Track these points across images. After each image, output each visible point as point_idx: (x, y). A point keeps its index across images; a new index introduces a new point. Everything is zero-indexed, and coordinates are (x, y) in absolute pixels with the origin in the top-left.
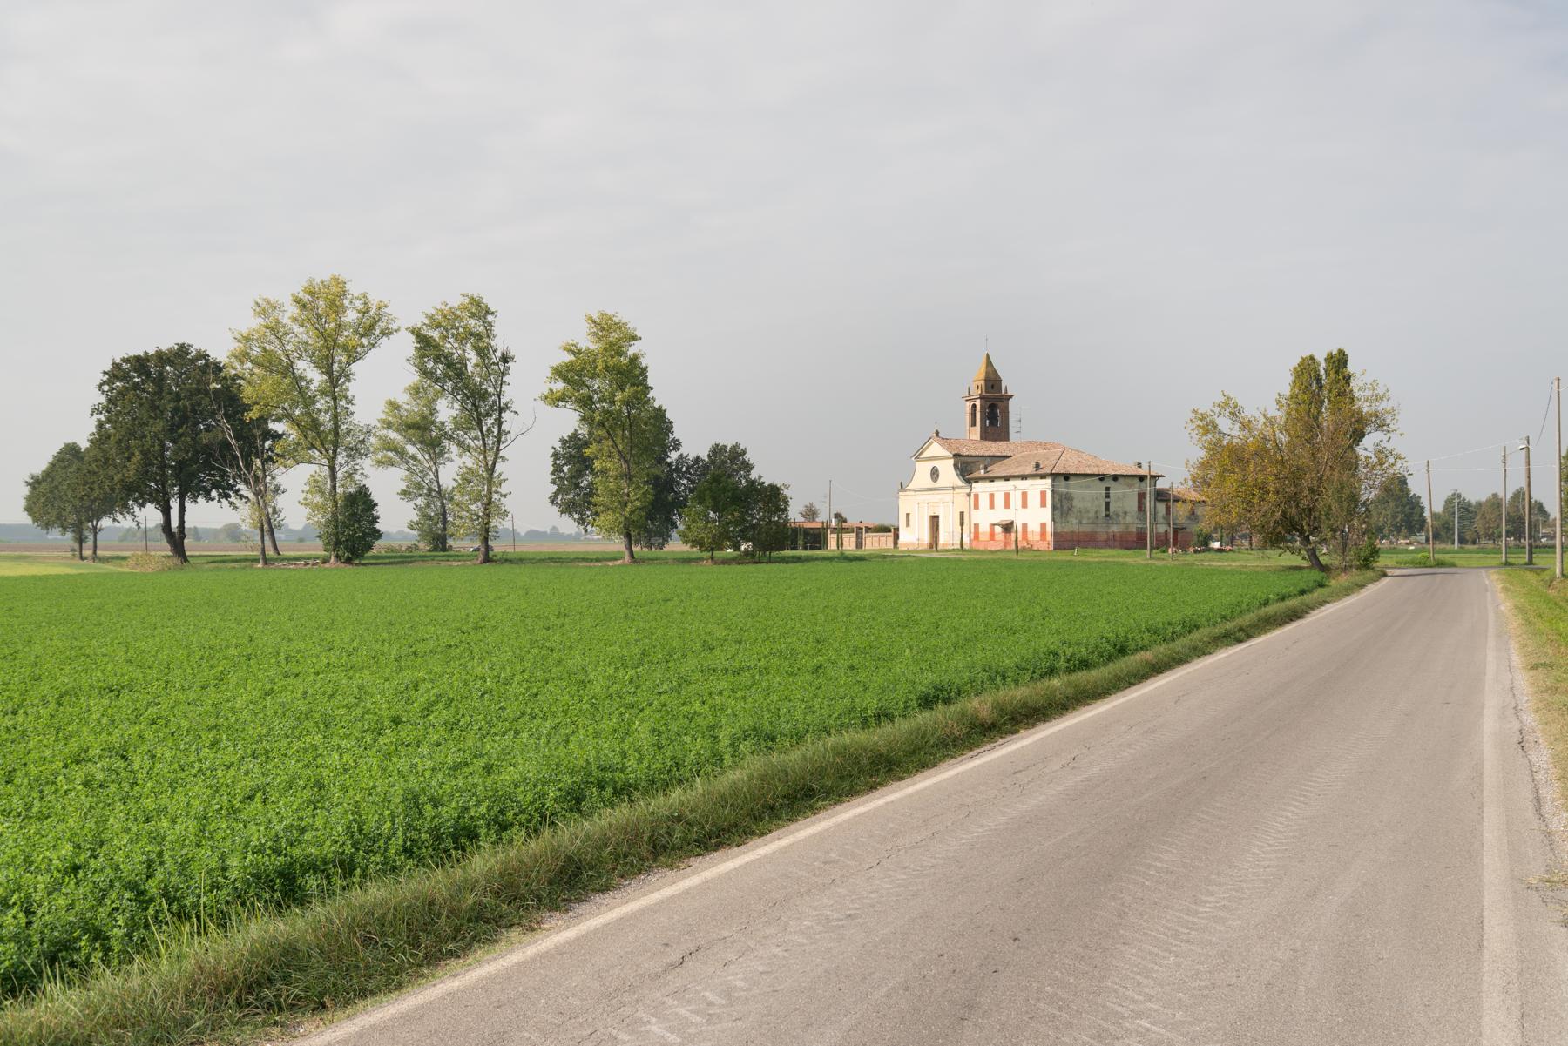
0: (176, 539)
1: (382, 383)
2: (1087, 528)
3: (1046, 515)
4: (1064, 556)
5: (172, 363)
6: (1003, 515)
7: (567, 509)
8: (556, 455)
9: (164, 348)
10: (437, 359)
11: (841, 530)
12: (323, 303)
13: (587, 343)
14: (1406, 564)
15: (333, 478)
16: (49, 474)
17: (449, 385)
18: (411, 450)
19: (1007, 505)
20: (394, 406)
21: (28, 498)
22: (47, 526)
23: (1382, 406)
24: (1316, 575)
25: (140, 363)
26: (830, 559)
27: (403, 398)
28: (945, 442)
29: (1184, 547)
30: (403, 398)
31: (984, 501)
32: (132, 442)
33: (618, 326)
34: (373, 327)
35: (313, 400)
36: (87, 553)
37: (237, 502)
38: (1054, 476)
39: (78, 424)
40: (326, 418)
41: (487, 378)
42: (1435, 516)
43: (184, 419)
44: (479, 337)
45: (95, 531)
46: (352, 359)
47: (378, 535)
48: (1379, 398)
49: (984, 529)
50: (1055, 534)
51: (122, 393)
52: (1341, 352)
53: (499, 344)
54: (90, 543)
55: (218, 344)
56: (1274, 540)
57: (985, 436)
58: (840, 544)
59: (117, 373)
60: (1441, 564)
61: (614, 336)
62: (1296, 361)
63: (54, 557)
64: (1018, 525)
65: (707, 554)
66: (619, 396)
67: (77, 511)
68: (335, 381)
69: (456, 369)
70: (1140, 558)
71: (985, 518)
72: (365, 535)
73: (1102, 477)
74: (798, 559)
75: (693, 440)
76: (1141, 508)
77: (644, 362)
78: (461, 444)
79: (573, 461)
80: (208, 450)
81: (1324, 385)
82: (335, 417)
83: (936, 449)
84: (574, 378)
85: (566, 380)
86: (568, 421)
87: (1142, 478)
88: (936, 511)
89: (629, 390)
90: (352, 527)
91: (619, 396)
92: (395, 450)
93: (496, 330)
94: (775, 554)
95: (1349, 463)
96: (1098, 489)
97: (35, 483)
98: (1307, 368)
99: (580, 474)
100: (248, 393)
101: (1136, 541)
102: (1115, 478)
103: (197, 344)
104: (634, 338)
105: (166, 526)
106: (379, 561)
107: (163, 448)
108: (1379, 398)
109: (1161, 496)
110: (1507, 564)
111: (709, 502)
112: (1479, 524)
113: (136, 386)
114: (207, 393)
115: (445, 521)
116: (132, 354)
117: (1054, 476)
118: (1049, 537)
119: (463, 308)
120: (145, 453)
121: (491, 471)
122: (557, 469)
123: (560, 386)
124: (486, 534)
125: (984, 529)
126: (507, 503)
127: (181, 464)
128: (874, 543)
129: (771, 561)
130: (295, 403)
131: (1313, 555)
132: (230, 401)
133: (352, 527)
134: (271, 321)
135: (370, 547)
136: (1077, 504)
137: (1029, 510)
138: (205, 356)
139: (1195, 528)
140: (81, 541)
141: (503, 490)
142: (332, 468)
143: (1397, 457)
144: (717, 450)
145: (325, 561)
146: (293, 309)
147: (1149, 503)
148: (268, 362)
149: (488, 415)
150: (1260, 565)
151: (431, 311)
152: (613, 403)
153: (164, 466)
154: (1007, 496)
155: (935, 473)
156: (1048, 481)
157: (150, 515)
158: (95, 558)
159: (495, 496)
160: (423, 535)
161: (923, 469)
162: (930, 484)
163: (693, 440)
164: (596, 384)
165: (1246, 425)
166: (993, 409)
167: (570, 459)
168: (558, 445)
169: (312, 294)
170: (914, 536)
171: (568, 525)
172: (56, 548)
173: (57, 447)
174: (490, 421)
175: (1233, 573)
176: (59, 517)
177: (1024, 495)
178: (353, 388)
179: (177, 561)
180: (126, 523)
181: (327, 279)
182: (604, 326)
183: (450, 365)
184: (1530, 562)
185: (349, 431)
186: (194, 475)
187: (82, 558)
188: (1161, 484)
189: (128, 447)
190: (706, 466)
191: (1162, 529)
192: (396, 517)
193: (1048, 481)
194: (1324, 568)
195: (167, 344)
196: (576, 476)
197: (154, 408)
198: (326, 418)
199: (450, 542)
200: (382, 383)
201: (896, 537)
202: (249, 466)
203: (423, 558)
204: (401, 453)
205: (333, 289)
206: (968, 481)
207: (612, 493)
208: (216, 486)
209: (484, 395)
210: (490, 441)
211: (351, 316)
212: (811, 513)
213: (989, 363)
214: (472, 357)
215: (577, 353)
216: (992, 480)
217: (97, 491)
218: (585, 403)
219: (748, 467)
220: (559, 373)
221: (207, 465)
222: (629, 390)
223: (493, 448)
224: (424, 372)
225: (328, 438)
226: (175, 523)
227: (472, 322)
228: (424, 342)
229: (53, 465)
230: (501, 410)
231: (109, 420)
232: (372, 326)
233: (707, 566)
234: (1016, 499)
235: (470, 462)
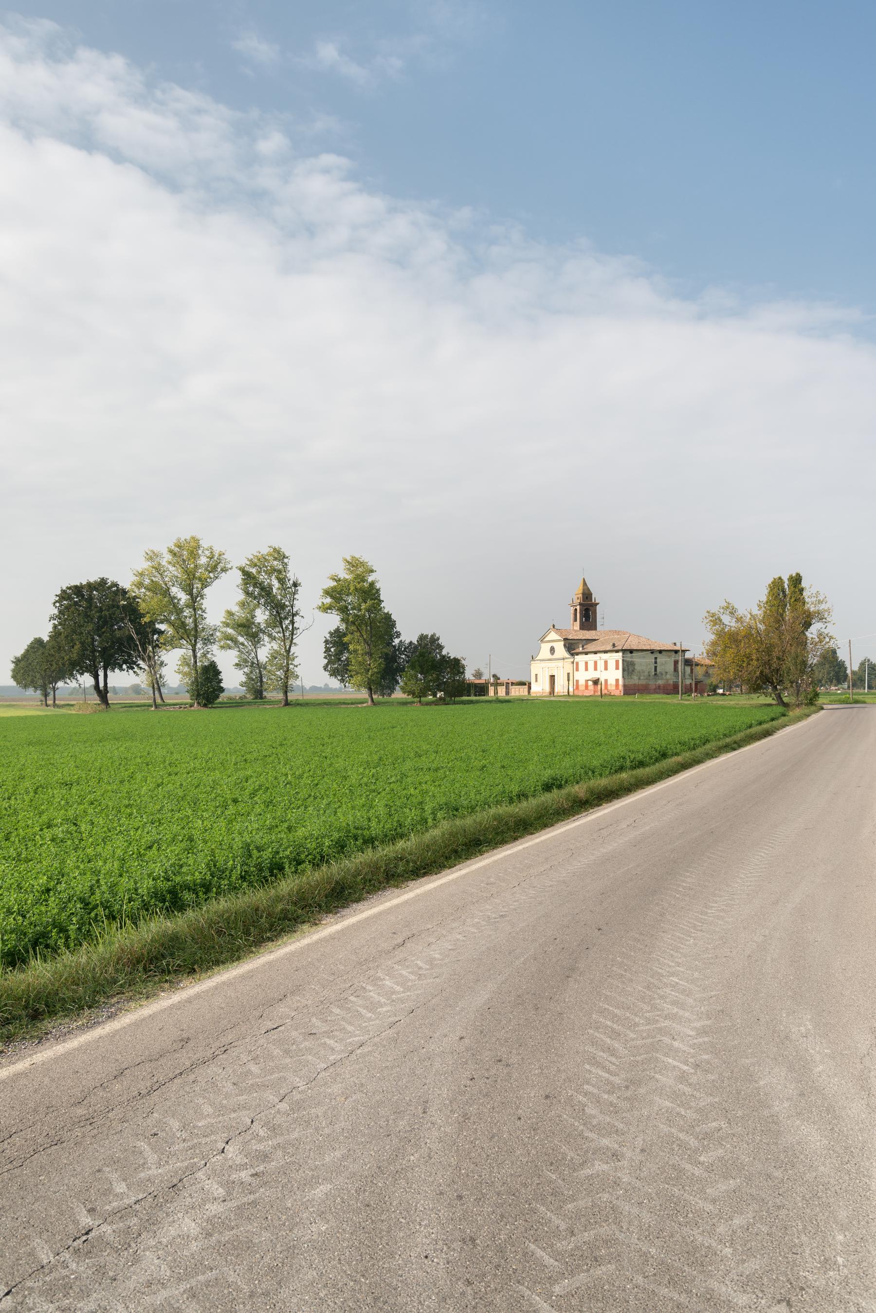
0: (103, 693)
1: (222, 600)
2: (643, 682)
3: (619, 674)
5: (97, 590)
6: (592, 674)
7: (334, 673)
8: (326, 642)
9: (92, 580)
10: (255, 586)
11: (497, 684)
12: (186, 552)
13: (344, 575)
15: (195, 656)
17: (263, 600)
18: (241, 639)
19: (596, 669)
20: (230, 614)
21: (13, 671)
22: (25, 687)
23: (822, 607)
24: (781, 709)
25: (77, 590)
26: (490, 702)
27: (235, 609)
28: (558, 631)
30: (235, 609)
31: (582, 666)
33: (362, 564)
34: (216, 567)
35: (182, 611)
36: (50, 702)
37: (138, 671)
43: (105, 623)
44: (279, 572)
46: (205, 585)
47: (222, 690)
48: (820, 602)
49: (582, 682)
50: (625, 686)
51: (67, 608)
53: (292, 576)
54: (51, 696)
56: (756, 688)
57: (583, 627)
58: (496, 692)
59: (64, 596)
62: (770, 580)
63: (30, 705)
64: (602, 680)
66: (363, 606)
67: (43, 678)
69: (266, 591)
71: (582, 676)
72: (214, 690)
73: (652, 652)
74: (471, 702)
75: (408, 632)
76: (676, 669)
77: (378, 585)
78: (270, 636)
79: (337, 644)
80: (120, 641)
81: (788, 596)
82: (195, 621)
83: (553, 636)
84: (336, 596)
85: (332, 597)
87: (676, 652)
88: (552, 672)
89: (369, 602)
90: (207, 685)
92: (231, 640)
93: (289, 568)
94: (457, 699)
96: (650, 659)
98: (777, 585)
100: (143, 607)
101: (673, 689)
102: (660, 652)
103: (111, 578)
104: (372, 571)
107: (93, 640)
108: (820, 602)
109: (688, 662)
113: (76, 603)
114: (118, 607)
115: (261, 681)
116: (72, 584)
118: (621, 688)
120: (82, 643)
121: (288, 651)
122: (327, 650)
123: (328, 600)
124: (286, 689)
125: (582, 682)
126: (298, 671)
127: (104, 650)
128: (517, 692)
129: (455, 703)
130: (171, 613)
131: (779, 697)
132: (132, 611)
134: (155, 564)
136: (637, 667)
138: (116, 585)
140: (46, 695)
141: (296, 662)
142: (194, 651)
143: (831, 638)
144: (422, 638)
145: (191, 706)
146: (168, 557)
148: (154, 588)
149: (286, 618)
152: (360, 610)
153: (94, 651)
154: (596, 663)
155: (552, 650)
156: (620, 654)
157: (87, 680)
158: (55, 705)
159: (291, 666)
160: (249, 690)
161: (545, 648)
162: (549, 656)
163: (408, 632)
165: (739, 620)
166: (587, 612)
167: (335, 644)
168: (328, 636)
169: (179, 547)
170: (540, 688)
171: (335, 683)
173: (29, 640)
174: (287, 622)
176: (32, 681)
177: (606, 663)
178: (206, 603)
179: (104, 707)
180: (73, 684)
182: (353, 564)
183: (263, 589)
185: (204, 629)
186: (112, 656)
187: (47, 705)
188: (688, 655)
189: (72, 640)
191: (688, 682)
192: (233, 680)
193: (620, 654)
194: (786, 705)
195: (94, 578)
196: (339, 654)
197: (87, 616)
199: (265, 694)
200: (222, 600)
201: (530, 688)
203: (249, 703)
204: (235, 642)
206: (572, 655)
207: (360, 664)
208: (125, 662)
209: (283, 606)
211: (203, 560)
212: (478, 675)
213: (585, 584)
214: (276, 584)
216: (586, 653)
217: (55, 666)
218: (343, 610)
219: (441, 647)
220: (327, 593)
221: (120, 650)
223: (289, 639)
224: (247, 593)
225: (191, 633)
226: (101, 685)
227: (275, 563)
228: (248, 577)
229: (27, 651)
230: (294, 615)
231: (60, 624)
232: (216, 567)
234: (601, 665)
235: (276, 647)
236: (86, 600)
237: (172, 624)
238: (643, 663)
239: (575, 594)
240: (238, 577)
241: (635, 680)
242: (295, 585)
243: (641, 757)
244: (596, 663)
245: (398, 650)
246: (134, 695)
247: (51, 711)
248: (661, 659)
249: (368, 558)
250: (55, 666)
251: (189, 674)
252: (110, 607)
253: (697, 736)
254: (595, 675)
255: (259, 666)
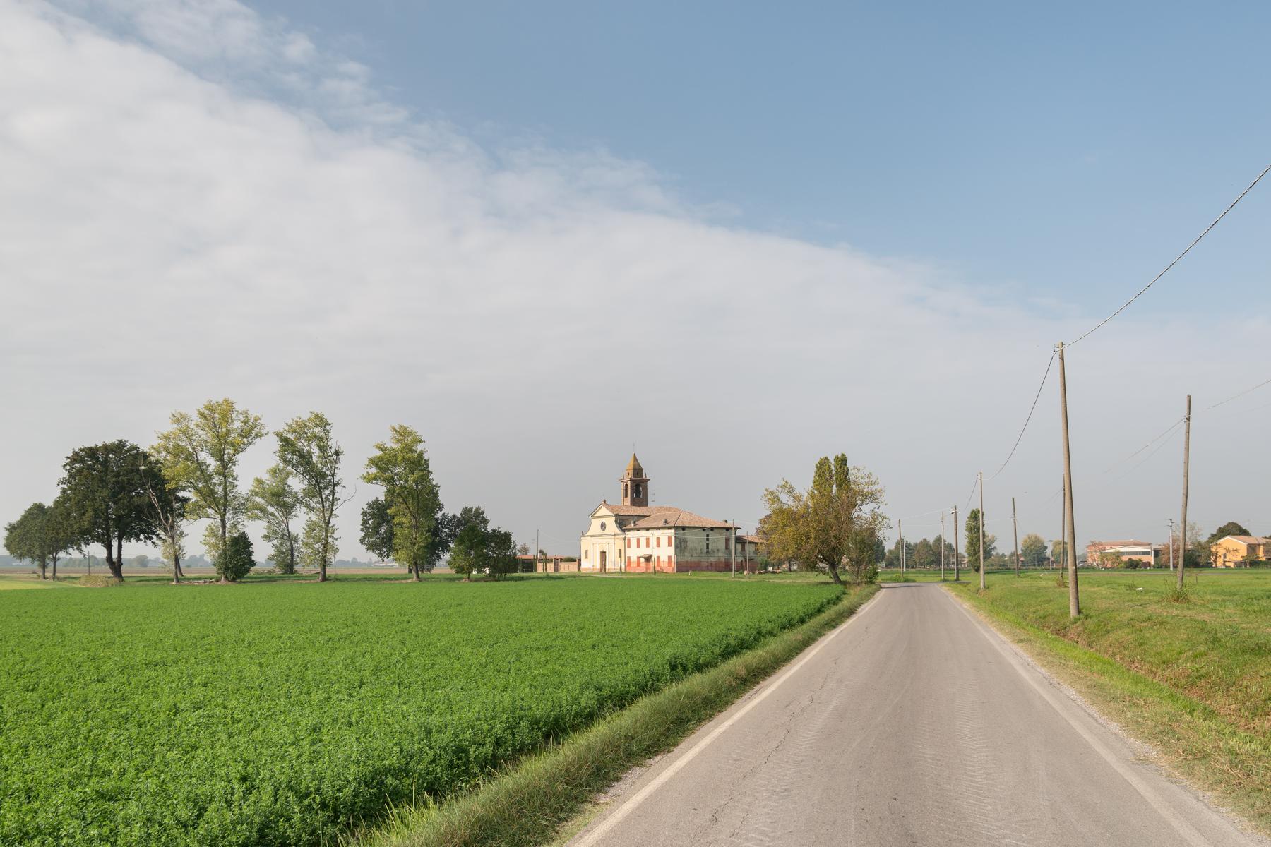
0: (116, 566)
1: (255, 466)
2: (695, 559)
3: (671, 551)
4: (683, 576)
5: (113, 451)
6: (644, 551)
7: (371, 547)
8: (364, 513)
9: (108, 442)
10: (293, 453)
11: (545, 560)
12: (217, 416)
13: (391, 444)
14: (895, 581)
15: (224, 527)
16: (23, 522)
17: (301, 469)
18: (270, 509)
19: (648, 545)
20: (259, 482)
21: (7, 539)
22: (21, 557)
23: (875, 488)
24: (840, 587)
25: (92, 452)
26: (542, 578)
27: (265, 477)
28: (609, 507)
29: (753, 570)
30: (265, 477)
31: (633, 542)
32: (87, 503)
33: (410, 434)
34: (250, 432)
35: (210, 477)
36: (48, 574)
37: (158, 542)
38: (676, 528)
39: (47, 486)
40: (219, 490)
41: (325, 465)
42: (890, 551)
43: (122, 488)
44: (320, 439)
45: (55, 560)
46: (237, 452)
47: (253, 563)
48: (873, 483)
49: (634, 559)
50: (677, 563)
51: (79, 472)
52: (843, 455)
53: (333, 444)
54: (51, 567)
55: (146, 440)
56: (811, 567)
57: (633, 503)
58: (545, 569)
59: (76, 458)
60: (907, 581)
61: (409, 439)
62: (817, 461)
63: (23, 578)
64: (654, 556)
65: (465, 575)
66: (411, 478)
67: (42, 548)
68: (225, 467)
69: (305, 459)
70: (730, 577)
71: (634, 553)
72: (245, 563)
73: (704, 529)
74: (522, 579)
75: (451, 506)
76: (727, 547)
77: (426, 457)
78: (308, 506)
79: (378, 515)
80: (139, 510)
81: (834, 474)
82: (225, 489)
83: (604, 511)
84: (383, 465)
85: (378, 466)
86: (379, 492)
87: (728, 529)
88: (602, 548)
89: (417, 474)
90: (236, 559)
91: (411, 478)
92: (260, 510)
93: (331, 435)
94: (508, 575)
95: (850, 520)
96: (702, 536)
97: (12, 529)
98: (823, 464)
99: (379, 525)
100: (167, 473)
101: (726, 567)
102: (712, 529)
103: (131, 441)
104: (421, 441)
105: (109, 558)
106: (253, 580)
107: (108, 507)
108: (873, 483)
109: (739, 540)
110: (945, 580)
111: (468, 544)
112: (916, 557)
113: (89, 467)
114: (138, 471)
115: (292, 555)
116: (87, 446)
117: (676, 528)
118: (673, 565)
119: (310, 420)
120: (95, 510)
121: (328, 523)
122: (365, 522)
123: (374, 470)
124: (324, 563)
125: (634, 559)
126: (338, 544)
127: (120, 517)
128: (565, 568)
129: (505, 580)
130: (199, 479)
131: (836, 576)
132: (154, 476)
133: (236, 559)
134: (183, 427)
135: (248, 571)
136: (690, 545)
137: (660, 548)
138: (136, 448)
139: (759, 559)
140: (44, 566)
141: (335, 535)
142: (223, 521)
143: (884, 518)
144: (466, 511)
145: (218, 581)
146: (196, 419)
147: (732, 542)
148: (178, 452)
149: (326, 488)
150: (800, 585)
151: (290, 422)
152: (407, 481)
153: (108, 519)
154: (648, 540)
155: (603, 526)
156: (673, 531)
157: (96, 550)
158: (54, 578)
159: (330, 539)
160: (278, 564)
161: (596, 523)
162: (600, 532)
163: (451, 506)
164: (397, 470)
165: (797, 498)
166: (638, 488)
167: (373, 516)
168: (366, 508)
169: (210, 410)
170: (590, 564)
171: (372, 556)
172: (23, 571)
173: (27, 506)
174: (327, 492)
175: (788, 586)
176: (29, 551)
177: (658, 539)
178: (237, 470)
179: (117, 580)
180: (75, 553)
181: (221, 400)
182: (402, 433)
183: (301, 456)
184: (958, 579)
185: (235, 498)
186: (128, 525)
187: (45, 578)
188: (739, 533)
189: (83, 506)
190: (459, 520)
191: (740, 559)
192: (263, 553)
193: (673, 531)
194: (844, 583)
195: (111, 440)
196: (376, 528)
197: (102, 481)
198: (219, 490)
199: (296, 568)
200: (255, 466)
201: (580, 564)
202: (167, 519)
203: (281, 578)
204: (264, 511)
205: (225, 407)
206: (624, 531)
207: (406, 538)
208: (143, 532)
209: (324, 476)
210: (327, 505)
211: (237, 425)
212: (525, 550)
213: (635, 459)
214: (316, 452)
215: (384, 450)
216: (638, 530)
217: (62, 535)
218: (389, 481)
219: (485, 521)
220: (374, 462)
221: (138, 519)
222: (417, 474)
223: (328, 510)
224: (285, 461)
225: (220, 501)
226: (115, 555)
227: (317, 430)
228: (285, 442)
229: (25, 517)
230: (335, 485)
231: (70, 488)
232: (250, 432)
233: (465, 583)
234: (653, 542)
235: (314, 518)
236: (101, 464)
237: (198, 491)
238: (695, 540)
239: (626, 470)
240: (276, 444)
241: (687, 557)
242: (337, 453)
243: (743, 634)
244: (648, 540)
245: (439, 523)
246: (139, 568)
247: (50, 585)
248: (713, 536)
249: (418, 429)
250: (62, 535)
251: (215, 546)
252: (128, 472)
253: (781, 614)
254: (647, 552)
255: (291, 538)
